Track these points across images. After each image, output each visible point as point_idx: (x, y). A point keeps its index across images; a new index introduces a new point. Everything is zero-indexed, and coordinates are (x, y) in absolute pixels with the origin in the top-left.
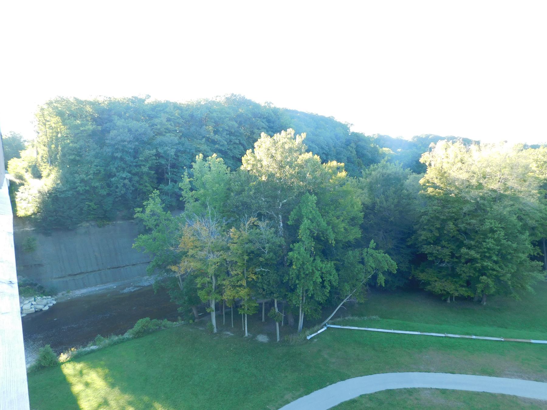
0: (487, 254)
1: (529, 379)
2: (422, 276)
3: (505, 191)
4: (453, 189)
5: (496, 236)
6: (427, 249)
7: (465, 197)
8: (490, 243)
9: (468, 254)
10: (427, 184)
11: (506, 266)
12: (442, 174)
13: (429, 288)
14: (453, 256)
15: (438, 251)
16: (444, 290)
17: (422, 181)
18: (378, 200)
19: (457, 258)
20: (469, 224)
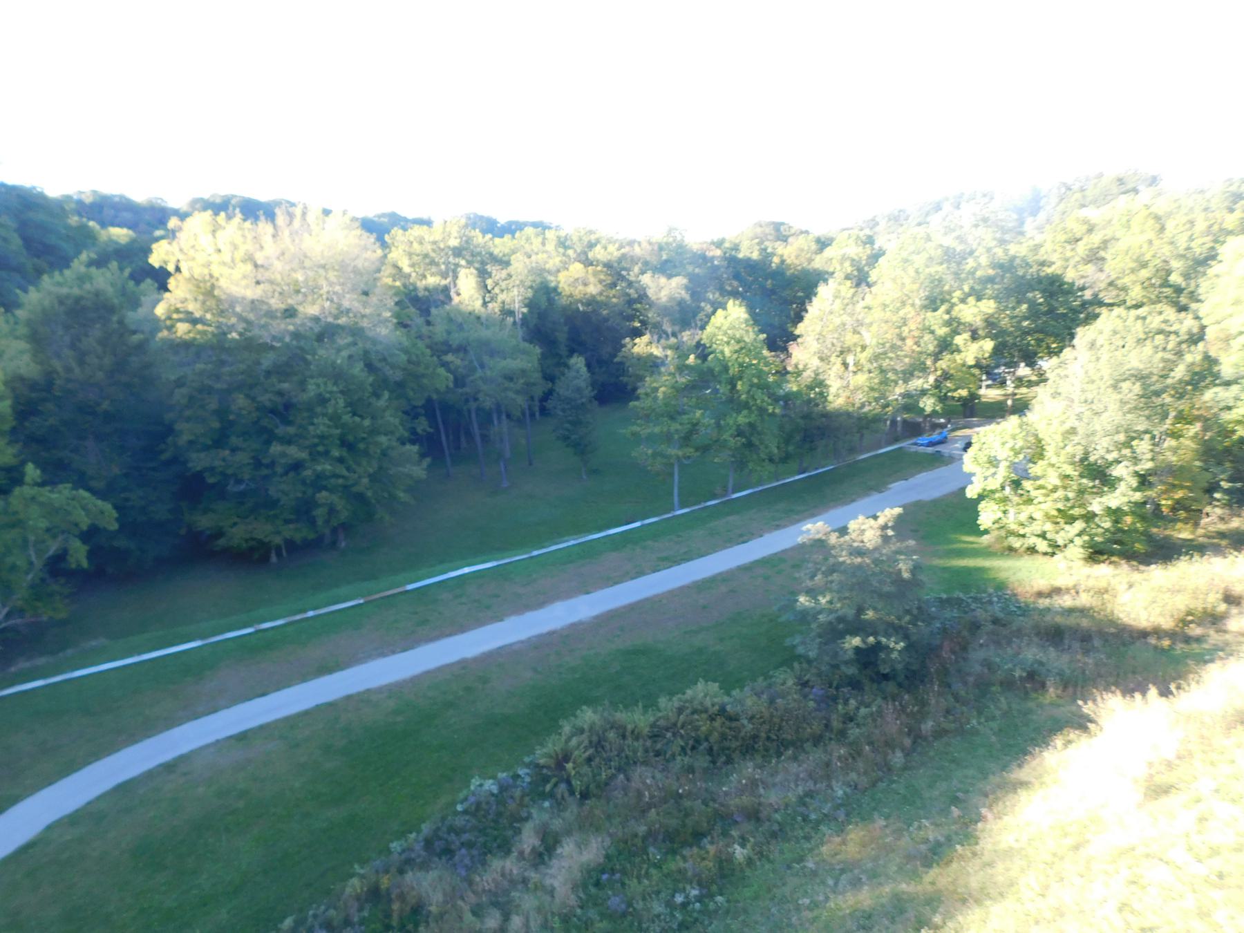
0: (320, 449)
1: (394, 652)
2: (204, 522)
3: (336, 317)
4: (234, 320)
5: (330, 411)
6: (198, 461)
7: (261, 337)
8: (321, 425)
9: (284, 455)
10: (175, 316)
11: (359, 464)
12: (207, 290)
13: (222, 542)
14: (258, 464)
15: (224, 460)
16: (253, 539)
17: (160, 310)
18: (57, 364)
19: (267, 466)
20: (280, 393)
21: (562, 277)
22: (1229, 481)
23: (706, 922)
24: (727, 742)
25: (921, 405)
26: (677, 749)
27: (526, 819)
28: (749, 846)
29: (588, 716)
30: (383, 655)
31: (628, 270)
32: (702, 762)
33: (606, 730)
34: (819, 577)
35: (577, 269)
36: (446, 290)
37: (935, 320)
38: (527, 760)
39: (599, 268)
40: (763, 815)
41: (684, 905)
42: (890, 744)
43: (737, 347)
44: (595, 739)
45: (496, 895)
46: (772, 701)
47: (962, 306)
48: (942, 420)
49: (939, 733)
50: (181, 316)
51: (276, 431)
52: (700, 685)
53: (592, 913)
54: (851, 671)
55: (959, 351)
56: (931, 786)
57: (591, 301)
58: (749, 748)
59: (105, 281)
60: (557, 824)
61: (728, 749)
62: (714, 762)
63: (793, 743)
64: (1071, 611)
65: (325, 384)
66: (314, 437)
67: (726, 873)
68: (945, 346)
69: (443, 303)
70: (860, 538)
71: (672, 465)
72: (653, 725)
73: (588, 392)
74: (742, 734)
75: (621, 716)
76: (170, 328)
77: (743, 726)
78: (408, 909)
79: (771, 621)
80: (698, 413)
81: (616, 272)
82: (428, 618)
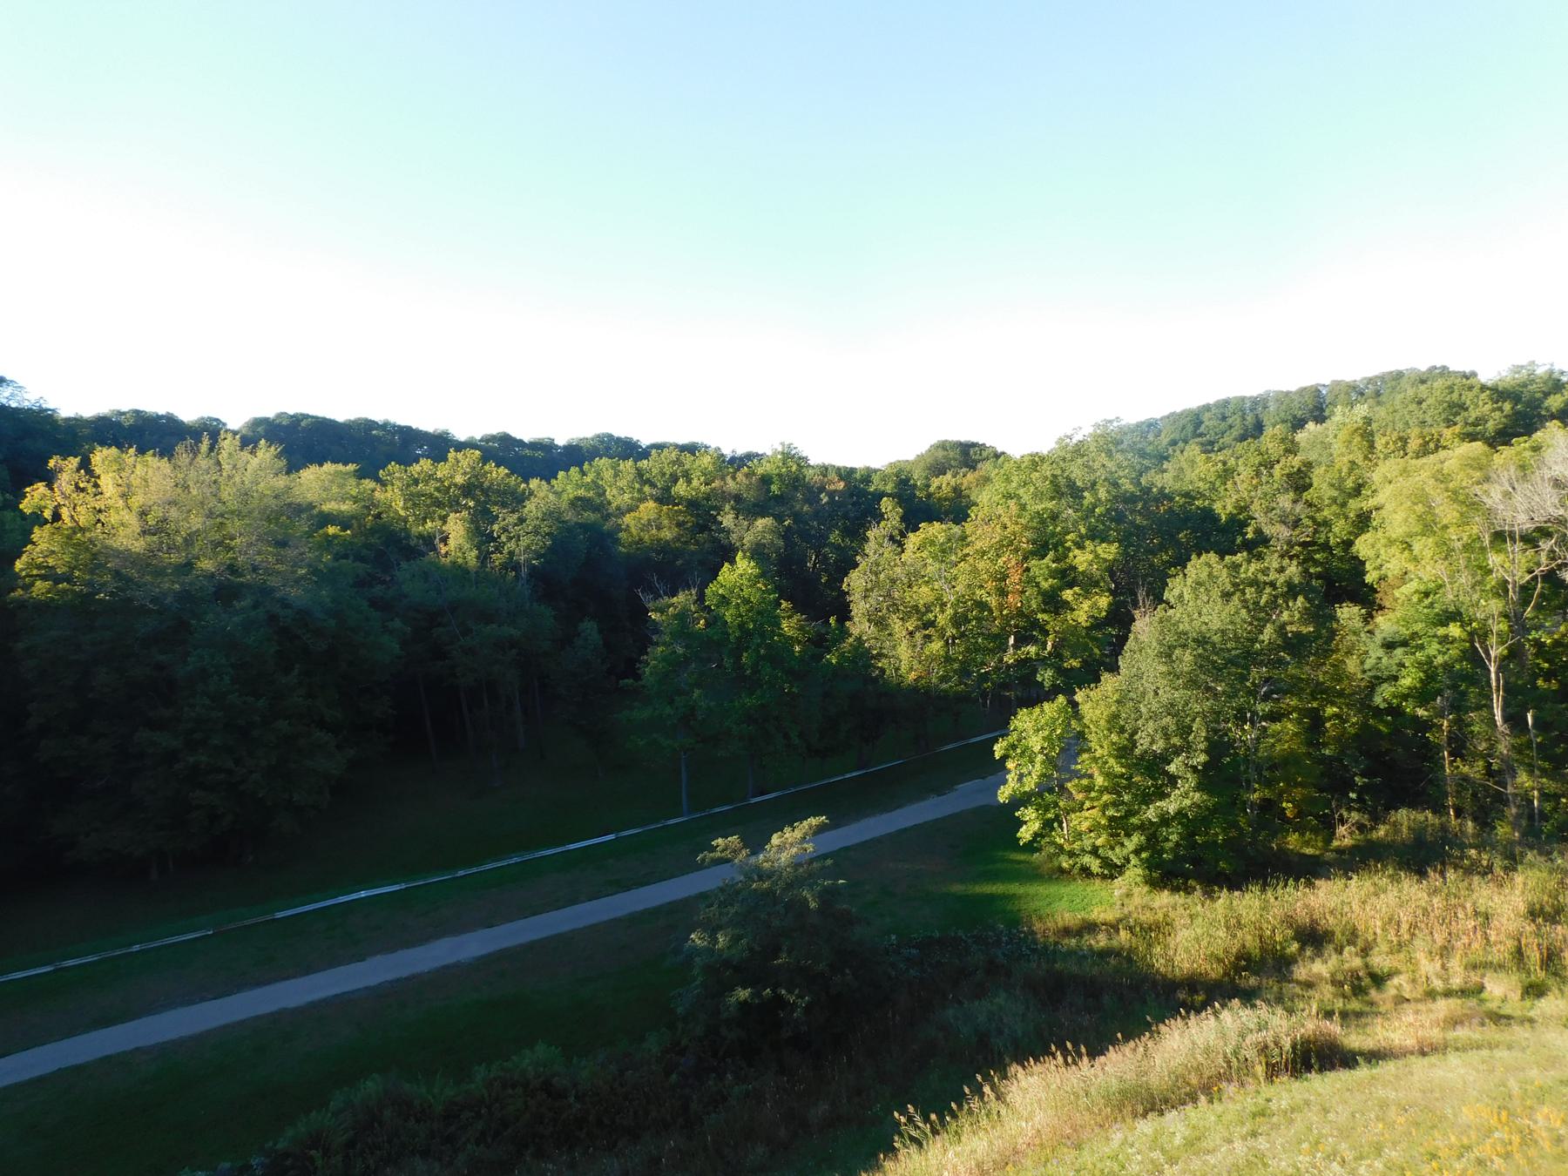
4: (107, 578)
21: (628, 519)
22: (1363, 775)
35: (649, 509)
37: (1042, 568)
64: (1105, 954)
68: (1053, 603)
80: (697, 693)
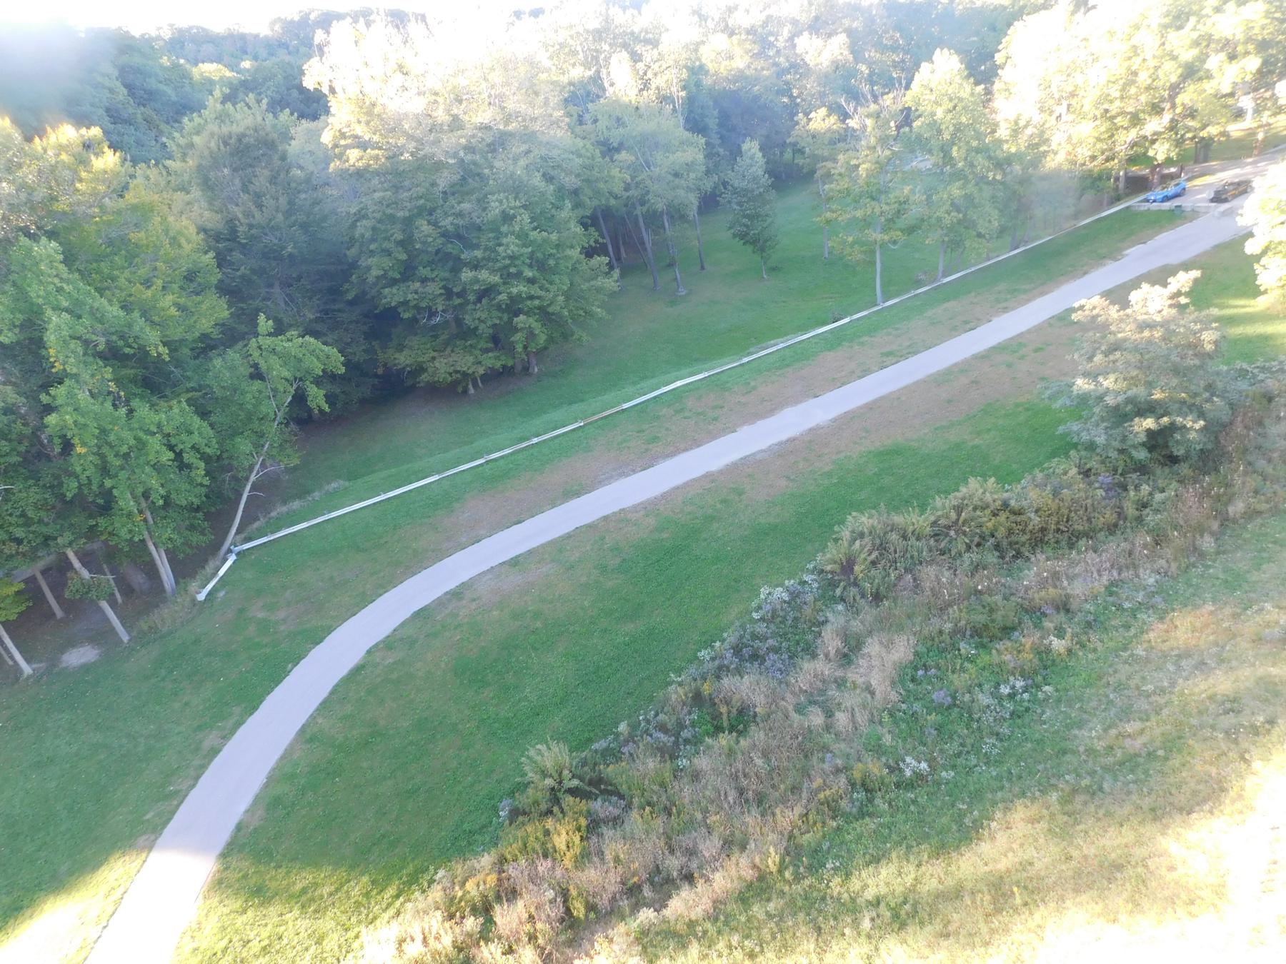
0: (512, 270)
1: (634, 471)
2: (403, 359)
4: (402, 141)
5: (517, 228)
6: (392, 296)
8: (511, 245)
10: (343, 142)
12: (369, 111)
14: (449, 294)
15: (416, 293)
16: (457, 372)
17: (327, 138)
18: (238, 212)
19: (459, 295)
23: (1039, 711)
24: (1016, 540)
25: (1151, 153)
26: (962, 547)
27: (826, 622)
28: (1068, 636)
29: (865, 521)
30: (624, 475)
31: (776, 35)
32: (992, 558)
33: (886, 533)
34: (1098, 358)
35: (719, 42)
36: (596, 79)
38: (810, 566)
39: (743, 37)
40: (1074, 605)
41: (1011, 696)
42: (1201, 530)
43: (951, 106)
44: (878, 541)
45: (811, 694)
46: (1056, 493)
47: (1218, 17)
48: (1173, 170)
49: (1252, 514)
50: (349, 141)
51: (463, 256)
52: (974, 483)
53: (917, 706)
54: (1142, 455)
55: (1209, 76)
56: (1258, 567)
57: (740, 76)
58: (1039, 540)
59: (248, 117)
60: (856, 626)
61: (1017, 543)
62: (1002, 557)
63: (1086, 535)
65: (507, 199)
66: (504, 258)
67: (1046, 665)
69: (598, 97)
70: (1144, 310)
71: (873, 252)
72: (934, 523)
73: (766, 180)
74: (1030, 527)
75: (898, 519)
76: (340, 156)
77: (1030, 519)
78: (734, 711)
79: (1027, 410)
81: (761, 39)
82: (655, 435)
